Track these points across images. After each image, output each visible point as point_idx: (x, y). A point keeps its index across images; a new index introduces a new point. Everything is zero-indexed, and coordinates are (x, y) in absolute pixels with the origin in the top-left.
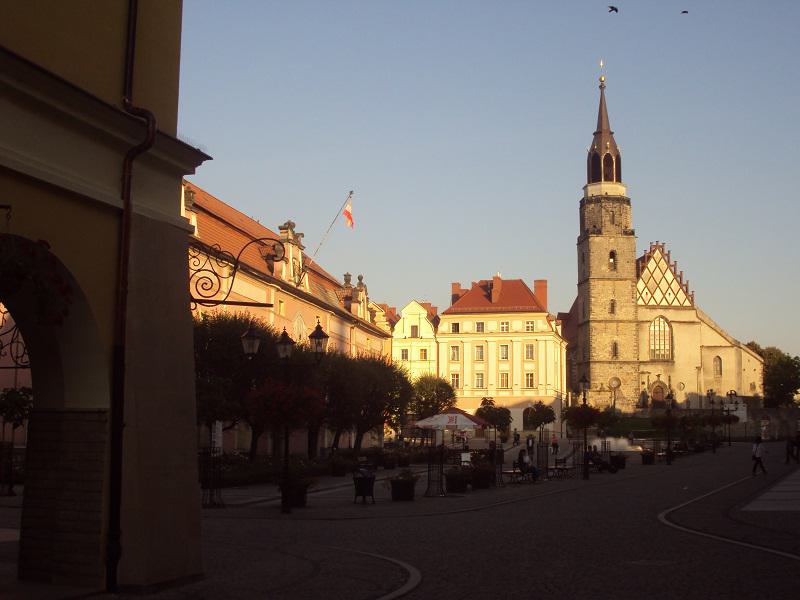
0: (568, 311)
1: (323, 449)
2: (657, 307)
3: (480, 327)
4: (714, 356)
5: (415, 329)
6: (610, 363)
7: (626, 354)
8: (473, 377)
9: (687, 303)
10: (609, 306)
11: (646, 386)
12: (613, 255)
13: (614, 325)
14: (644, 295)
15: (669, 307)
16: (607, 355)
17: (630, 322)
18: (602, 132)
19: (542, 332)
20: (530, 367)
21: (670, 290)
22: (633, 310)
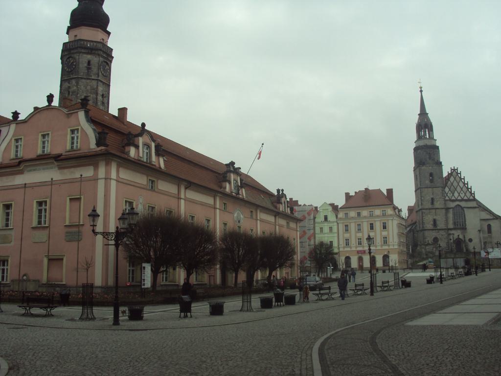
0: (413, 205)
1: (257, 281)
2: (456, 200)
3: (359, 214)
4: (487, 224)
5: (326, 218)
6: (433, 230)
7: (441, 225)
8: (381, 239)
9: (471, 198)
10: (430, 201)
11: (452, 241)
12: (431, 175)
13: (434, 211)
14: (449, 195)
15: (462, 200)
16: (431, 226)
17: (443, 208)
18: (423, 114)
19: (378, 216)
20: (385, 233)
21: (462, 192)
22: (444, 202)
